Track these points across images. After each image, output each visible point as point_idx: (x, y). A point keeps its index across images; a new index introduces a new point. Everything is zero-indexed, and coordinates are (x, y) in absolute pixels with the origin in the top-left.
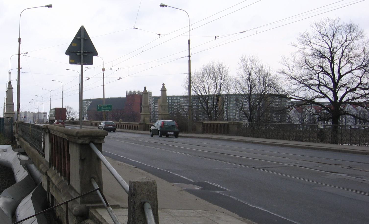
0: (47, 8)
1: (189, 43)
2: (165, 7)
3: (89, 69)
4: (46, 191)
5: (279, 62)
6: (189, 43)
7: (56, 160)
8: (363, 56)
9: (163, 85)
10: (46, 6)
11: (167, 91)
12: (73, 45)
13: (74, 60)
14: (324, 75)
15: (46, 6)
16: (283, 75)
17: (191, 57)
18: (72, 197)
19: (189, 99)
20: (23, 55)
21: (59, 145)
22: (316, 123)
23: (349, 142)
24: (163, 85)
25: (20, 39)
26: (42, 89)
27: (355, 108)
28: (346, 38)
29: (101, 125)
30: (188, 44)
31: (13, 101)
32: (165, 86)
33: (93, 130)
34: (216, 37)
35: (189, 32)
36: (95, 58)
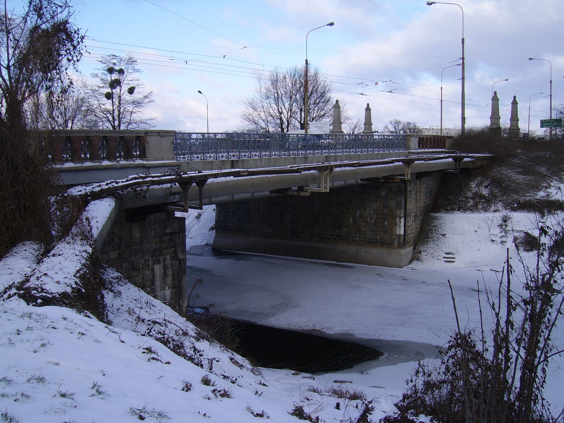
0: (329, 26)
1: (463, 43)
2: (433, 4)
3: (113, 305)
4: (463, 161)
5: (136, 325)
6: (463, 43)
7: (268, 256)
8: (10, 42)
9: (368, 104)
10: (328, 25)
11: (519, 121)
12: (52, 305)
13: (536, 416)
14: (63, 85)
15: (328, 25)
16: (349, 331)
17: (490, 114)
18: (205, 198)
19: (519, 149)
20: (488, 225)
21: (447, 155)
22: (518, 406)
23: (537, 299)
24: (368, 104)
25: (463, 40)
26: (61, 363)
27: (10, 61)
28: (70, 6)
29: (538, 168)
30: (550, 83)
31: (500, 115)
32: (497, 95)
33: (379, 170)
34: (224, 56)
35: (557, 352)
36: (185, 319)
